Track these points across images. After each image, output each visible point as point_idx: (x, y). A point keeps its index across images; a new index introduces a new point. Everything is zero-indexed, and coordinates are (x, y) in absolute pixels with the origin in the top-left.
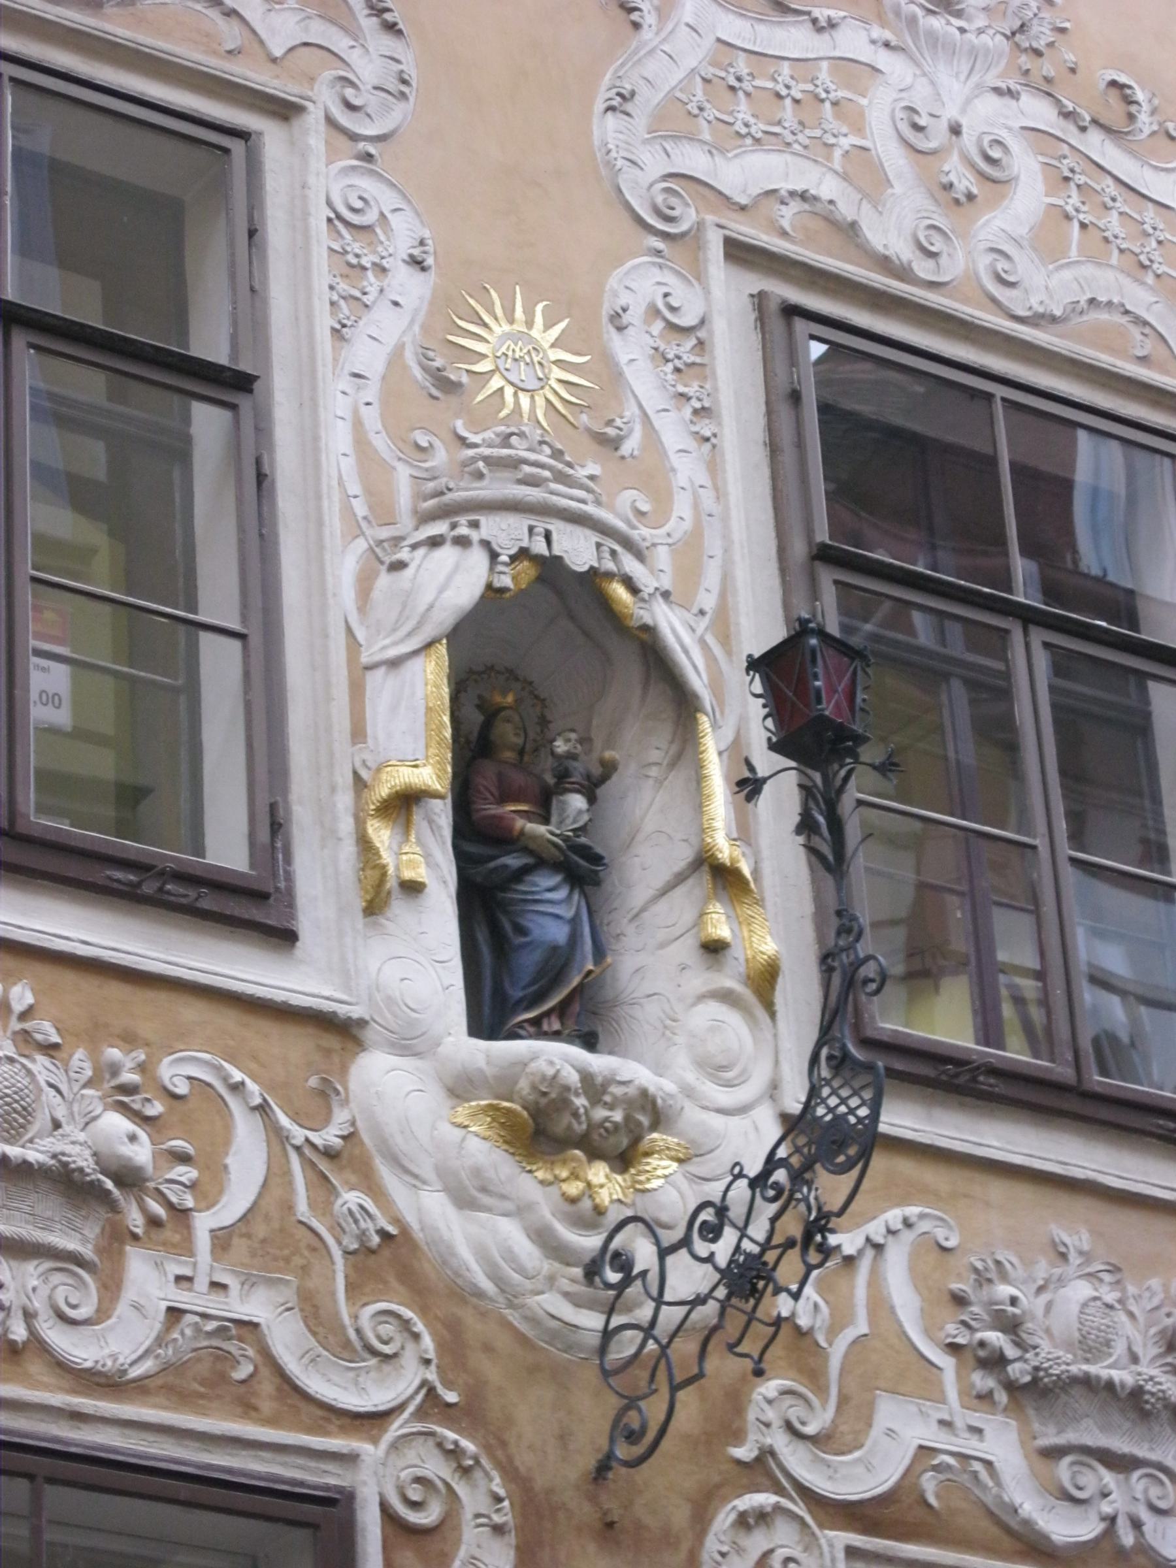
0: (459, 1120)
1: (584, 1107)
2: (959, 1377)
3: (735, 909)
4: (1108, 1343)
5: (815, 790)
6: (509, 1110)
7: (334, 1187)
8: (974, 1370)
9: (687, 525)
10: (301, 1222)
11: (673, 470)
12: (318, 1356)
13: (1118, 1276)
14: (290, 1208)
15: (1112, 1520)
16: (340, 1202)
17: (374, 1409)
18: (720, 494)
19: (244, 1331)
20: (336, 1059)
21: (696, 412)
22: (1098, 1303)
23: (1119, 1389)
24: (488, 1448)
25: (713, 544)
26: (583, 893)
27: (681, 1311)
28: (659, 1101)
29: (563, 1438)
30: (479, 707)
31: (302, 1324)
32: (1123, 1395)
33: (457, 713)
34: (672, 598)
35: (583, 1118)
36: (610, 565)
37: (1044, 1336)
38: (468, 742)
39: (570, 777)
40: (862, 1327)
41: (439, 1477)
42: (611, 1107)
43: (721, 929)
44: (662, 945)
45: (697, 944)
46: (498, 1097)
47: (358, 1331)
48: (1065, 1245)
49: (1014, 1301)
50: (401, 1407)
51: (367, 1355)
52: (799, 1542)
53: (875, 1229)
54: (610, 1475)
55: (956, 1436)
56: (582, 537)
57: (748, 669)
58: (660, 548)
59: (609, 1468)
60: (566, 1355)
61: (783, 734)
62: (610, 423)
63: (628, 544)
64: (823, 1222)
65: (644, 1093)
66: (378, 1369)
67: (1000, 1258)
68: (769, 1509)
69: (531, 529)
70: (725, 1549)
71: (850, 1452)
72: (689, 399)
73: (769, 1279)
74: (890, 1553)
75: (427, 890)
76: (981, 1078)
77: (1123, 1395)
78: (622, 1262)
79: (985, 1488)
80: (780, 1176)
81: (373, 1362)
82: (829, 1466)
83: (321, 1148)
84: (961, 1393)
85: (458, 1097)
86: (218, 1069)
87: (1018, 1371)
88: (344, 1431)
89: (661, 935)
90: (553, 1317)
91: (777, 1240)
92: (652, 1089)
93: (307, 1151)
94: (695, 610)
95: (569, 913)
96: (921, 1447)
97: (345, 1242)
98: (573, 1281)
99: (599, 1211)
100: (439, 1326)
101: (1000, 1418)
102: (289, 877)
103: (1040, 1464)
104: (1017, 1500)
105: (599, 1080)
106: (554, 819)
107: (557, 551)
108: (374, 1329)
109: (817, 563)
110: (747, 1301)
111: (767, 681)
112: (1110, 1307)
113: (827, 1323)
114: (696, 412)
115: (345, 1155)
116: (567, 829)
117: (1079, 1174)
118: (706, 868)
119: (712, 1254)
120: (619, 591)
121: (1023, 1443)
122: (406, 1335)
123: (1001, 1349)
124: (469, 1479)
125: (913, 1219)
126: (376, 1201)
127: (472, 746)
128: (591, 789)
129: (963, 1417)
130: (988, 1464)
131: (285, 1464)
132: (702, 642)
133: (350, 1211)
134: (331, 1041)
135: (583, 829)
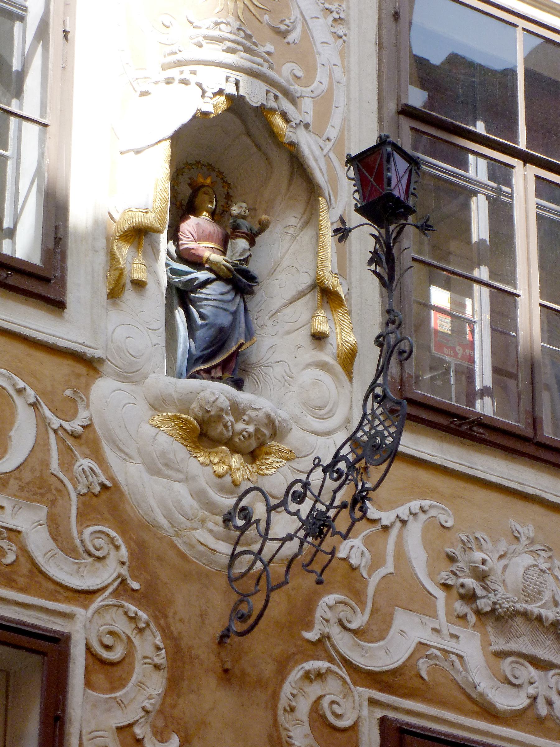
0: (154, 423)
1: (231, 422)
2: (447, 604)
3: (333, 315)
4: (540, 593)
5: (381, 239)
6: (186, 420)
7: (75, 455)
8: (457, 601)
9: (325, 87)
10: (53, 474)
11: (319, 53)
12: (56, 554)
13: (550, 554)
14: (48, 465)
15: (534, 698)
16: (78, 464)
17: (87, 588)
18: (347, 71)
19: (12, 535)
20: (83, 380)
21: (335, 20)
22: (536, 569)
23: (544, 620)
24: (156, 619)
25: (340, 98)
26: (242, 297)
27: (277, 544)
28: (277, 422)
29: (202, 615)
30: (190, 185)
31: (48, 533)
32: (547, 625)
33: (176, 188)
34: (311, 128)
35: (230, 428)
36: (272, 104)
37: (502, 585)
38: (181, 205)
39: (239, 229)
40: (389, 568)
41: (124, 632)
42: (248, 423)
43: (322, 326)
44: (289, 333)
45: (309, 334)
46: (179, 411)
47: (82, 541)
48: (518, 532)
49: (484, 562)
50: (104, 588)
51: (86, 556)
52: (341, 692)
53: (403, 511)
54: (229, 641)
55: (442, 638)
56: (258, 86)
57: (347, 163)
58: (306, 99)
59: (228, 636)
60: (208, 567)
61: (364, 203)
62: (282, 21)
63: (287, 93)
64: (364, 494)
65: (268, 416)
66: (92, 565)
67: (478, 535)
68: (324, 671)
69: (227, 79)
70: (295, 692)
71: (377, 641)
72: (332, 12)
73: (329, 527)
74: (396, 705)
75: (147, 287)
76: (475, 428)
77: (547, 625)
78: (245, 513)
79: (458, 671)
80: (342, 465)
81: (90, 560)
82: (363, 649)
83: (69, 431)
84: (448, 614)
85: (156, 410)
86: (10, 379)
87: (484, 604)
88: (67, 600)
89: (287, 327)
90: (202, 544)
91: (337, 503)
92: (273, 415)
93: (60, 432)
94: (324, 137)
95: (233, 308)
96: (420, 643)
97: (79, 489)
98: (216, 524)
99: (235, 484)
100: (132, 544)
101: (470, 630)
102: (63, 270)
103: (492, 658)
104: (477, 681)
105: (242, 406)
106: (229, 253)
107: (242, 93)
108: (92, 541)
109: (401, 116)
110: (316, 539)
111: (358, 171)
112: (544, 572)
113: (370, 563)
114: (335, 20)
115: (84, 437)
116: (236, 258)
117: (530, 491)
118: (318, 289)
119: (299, 510)
120: (278, 121)
121: (483, 648)
122: (111, 546)
123: (474, 589)
124: (142, 635)
125: (426, 508)
126: (100, 466)
127: (184, 207)
128: (251, 238)
129: (447, 628)
130: (461, 657)
131: (30, 616)
132: (326, 156)
133: (83, 470)
134: (81, 369)
135: (246, 260)
